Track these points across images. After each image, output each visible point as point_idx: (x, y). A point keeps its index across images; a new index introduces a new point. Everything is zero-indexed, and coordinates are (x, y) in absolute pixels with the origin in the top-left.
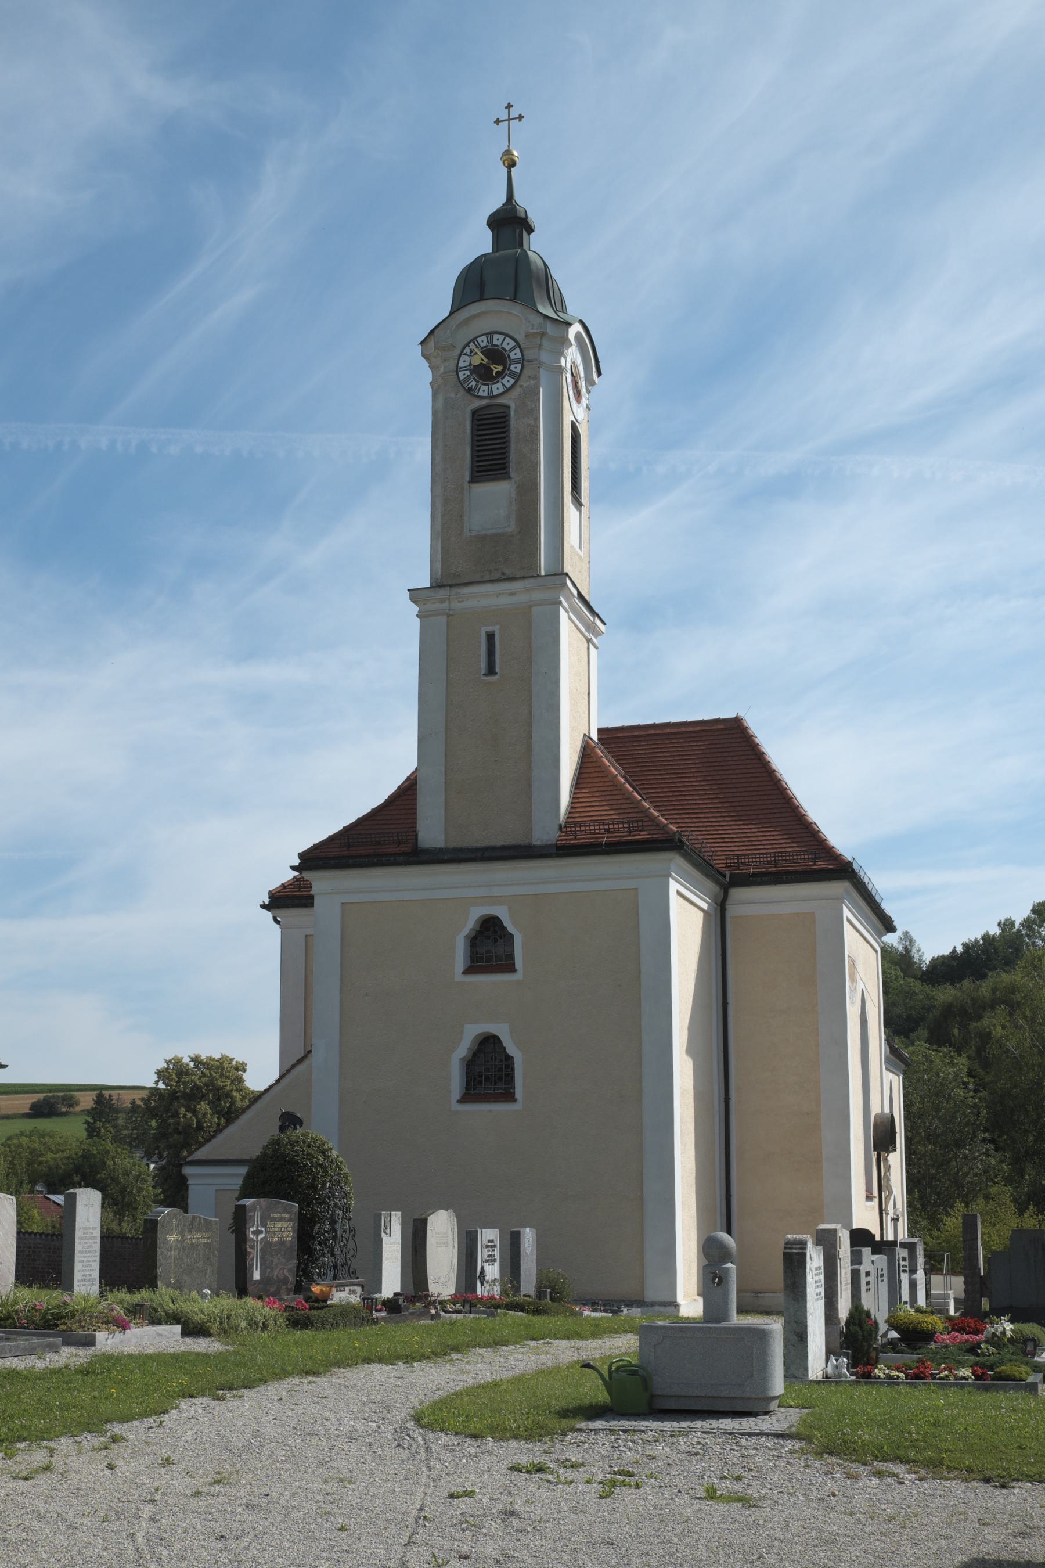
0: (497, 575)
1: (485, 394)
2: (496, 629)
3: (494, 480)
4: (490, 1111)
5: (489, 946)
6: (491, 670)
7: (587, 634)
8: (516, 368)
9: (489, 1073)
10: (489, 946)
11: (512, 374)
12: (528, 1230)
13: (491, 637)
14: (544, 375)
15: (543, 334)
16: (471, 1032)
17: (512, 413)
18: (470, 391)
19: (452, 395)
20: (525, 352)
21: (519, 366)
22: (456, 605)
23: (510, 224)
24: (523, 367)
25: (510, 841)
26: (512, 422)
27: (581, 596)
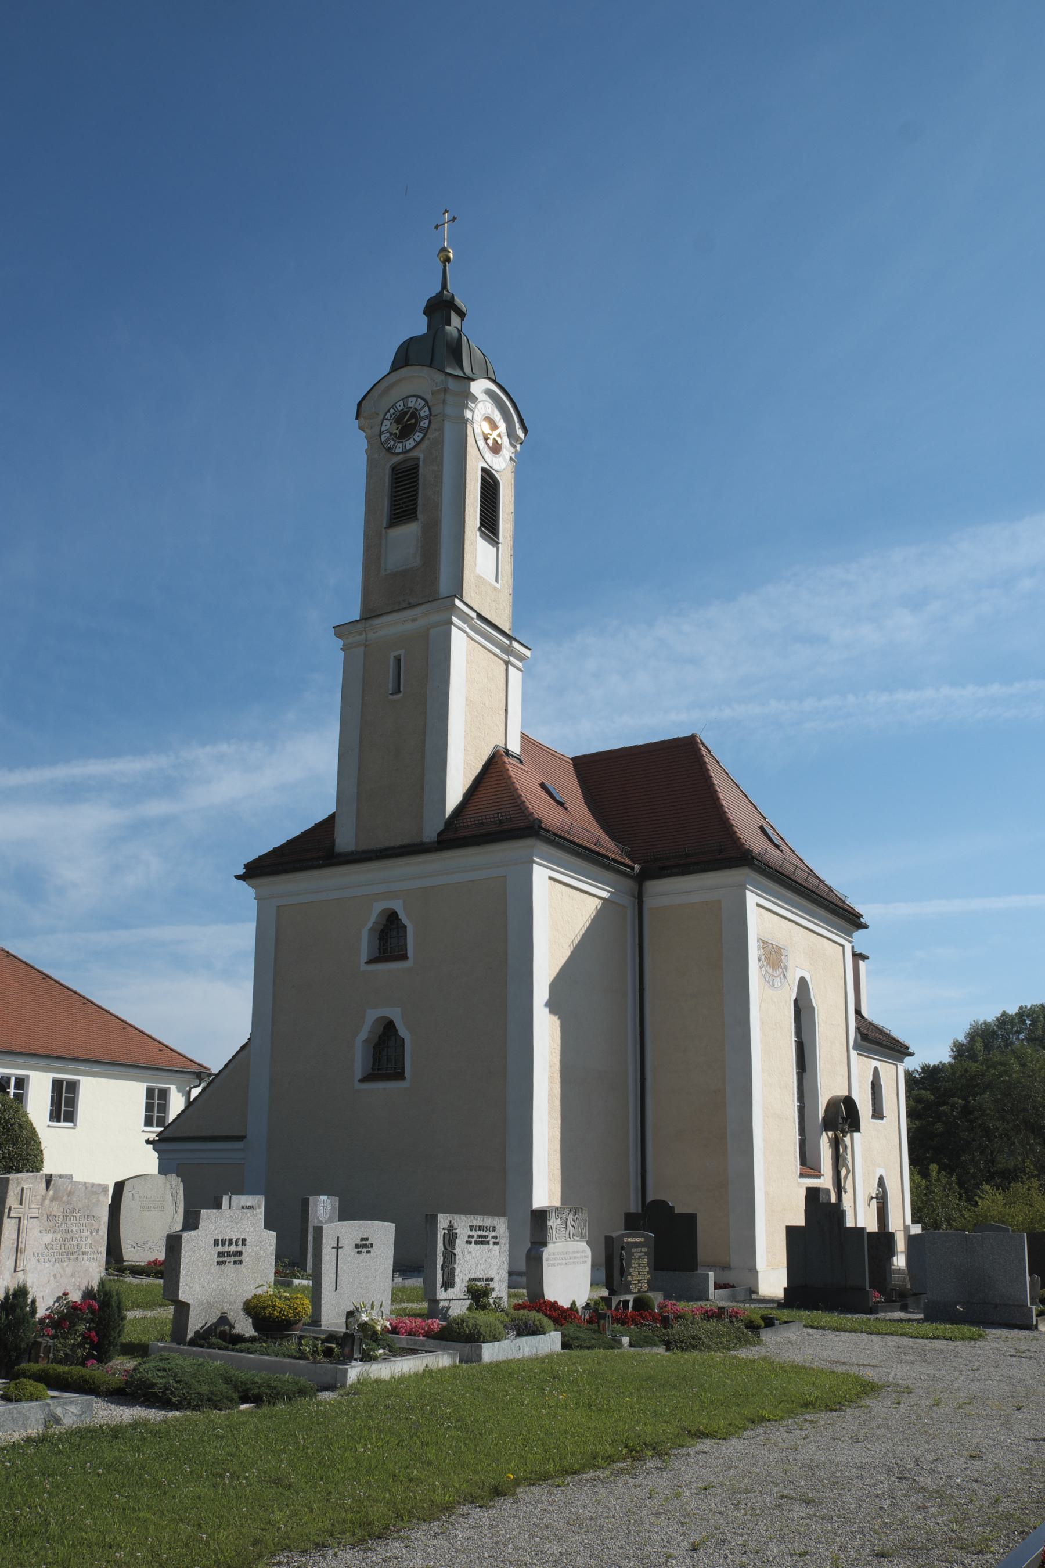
0: (405, 605)
1: (400, 450)
2: (402, 652)
3: (405, 523)
4: (385, 1089)
5: (389, 938)
6: (397, 690)
7: (505, 657)
8: (424, 424)
9: (386, 1056)
10: (389, 938)
11: (422, 429)
12: (324, 1198)
13: (398, 660)
14: (448, 426)
15: (445, 390)
16: (372, 1015)
17: (421, 463)
18: (389, 450)
19: (376, 456)
20: (433, 409)
21: (427, 421)
22: (371, 635)
23: (441, 308)
24: (430, 422)
25: (406, 841)
26: (421, 471)
27: (480, 616)
